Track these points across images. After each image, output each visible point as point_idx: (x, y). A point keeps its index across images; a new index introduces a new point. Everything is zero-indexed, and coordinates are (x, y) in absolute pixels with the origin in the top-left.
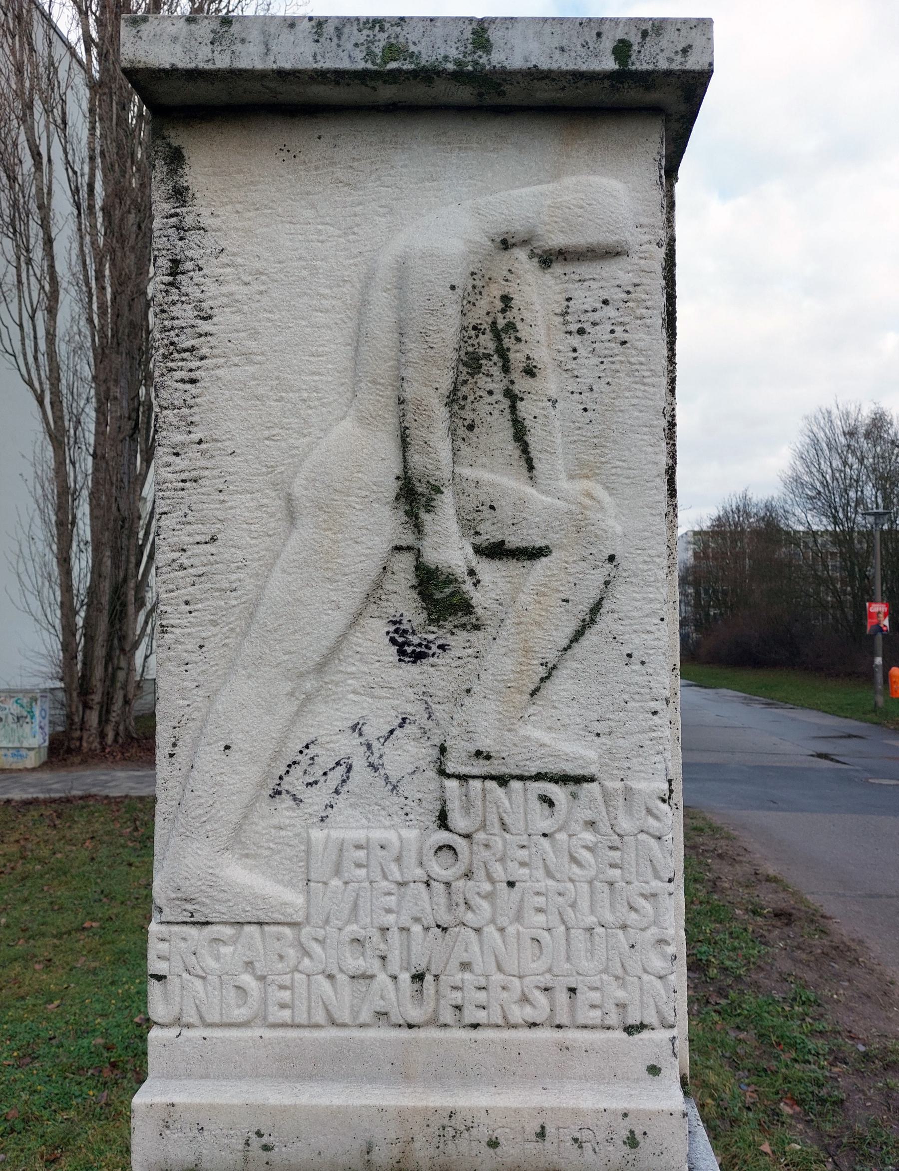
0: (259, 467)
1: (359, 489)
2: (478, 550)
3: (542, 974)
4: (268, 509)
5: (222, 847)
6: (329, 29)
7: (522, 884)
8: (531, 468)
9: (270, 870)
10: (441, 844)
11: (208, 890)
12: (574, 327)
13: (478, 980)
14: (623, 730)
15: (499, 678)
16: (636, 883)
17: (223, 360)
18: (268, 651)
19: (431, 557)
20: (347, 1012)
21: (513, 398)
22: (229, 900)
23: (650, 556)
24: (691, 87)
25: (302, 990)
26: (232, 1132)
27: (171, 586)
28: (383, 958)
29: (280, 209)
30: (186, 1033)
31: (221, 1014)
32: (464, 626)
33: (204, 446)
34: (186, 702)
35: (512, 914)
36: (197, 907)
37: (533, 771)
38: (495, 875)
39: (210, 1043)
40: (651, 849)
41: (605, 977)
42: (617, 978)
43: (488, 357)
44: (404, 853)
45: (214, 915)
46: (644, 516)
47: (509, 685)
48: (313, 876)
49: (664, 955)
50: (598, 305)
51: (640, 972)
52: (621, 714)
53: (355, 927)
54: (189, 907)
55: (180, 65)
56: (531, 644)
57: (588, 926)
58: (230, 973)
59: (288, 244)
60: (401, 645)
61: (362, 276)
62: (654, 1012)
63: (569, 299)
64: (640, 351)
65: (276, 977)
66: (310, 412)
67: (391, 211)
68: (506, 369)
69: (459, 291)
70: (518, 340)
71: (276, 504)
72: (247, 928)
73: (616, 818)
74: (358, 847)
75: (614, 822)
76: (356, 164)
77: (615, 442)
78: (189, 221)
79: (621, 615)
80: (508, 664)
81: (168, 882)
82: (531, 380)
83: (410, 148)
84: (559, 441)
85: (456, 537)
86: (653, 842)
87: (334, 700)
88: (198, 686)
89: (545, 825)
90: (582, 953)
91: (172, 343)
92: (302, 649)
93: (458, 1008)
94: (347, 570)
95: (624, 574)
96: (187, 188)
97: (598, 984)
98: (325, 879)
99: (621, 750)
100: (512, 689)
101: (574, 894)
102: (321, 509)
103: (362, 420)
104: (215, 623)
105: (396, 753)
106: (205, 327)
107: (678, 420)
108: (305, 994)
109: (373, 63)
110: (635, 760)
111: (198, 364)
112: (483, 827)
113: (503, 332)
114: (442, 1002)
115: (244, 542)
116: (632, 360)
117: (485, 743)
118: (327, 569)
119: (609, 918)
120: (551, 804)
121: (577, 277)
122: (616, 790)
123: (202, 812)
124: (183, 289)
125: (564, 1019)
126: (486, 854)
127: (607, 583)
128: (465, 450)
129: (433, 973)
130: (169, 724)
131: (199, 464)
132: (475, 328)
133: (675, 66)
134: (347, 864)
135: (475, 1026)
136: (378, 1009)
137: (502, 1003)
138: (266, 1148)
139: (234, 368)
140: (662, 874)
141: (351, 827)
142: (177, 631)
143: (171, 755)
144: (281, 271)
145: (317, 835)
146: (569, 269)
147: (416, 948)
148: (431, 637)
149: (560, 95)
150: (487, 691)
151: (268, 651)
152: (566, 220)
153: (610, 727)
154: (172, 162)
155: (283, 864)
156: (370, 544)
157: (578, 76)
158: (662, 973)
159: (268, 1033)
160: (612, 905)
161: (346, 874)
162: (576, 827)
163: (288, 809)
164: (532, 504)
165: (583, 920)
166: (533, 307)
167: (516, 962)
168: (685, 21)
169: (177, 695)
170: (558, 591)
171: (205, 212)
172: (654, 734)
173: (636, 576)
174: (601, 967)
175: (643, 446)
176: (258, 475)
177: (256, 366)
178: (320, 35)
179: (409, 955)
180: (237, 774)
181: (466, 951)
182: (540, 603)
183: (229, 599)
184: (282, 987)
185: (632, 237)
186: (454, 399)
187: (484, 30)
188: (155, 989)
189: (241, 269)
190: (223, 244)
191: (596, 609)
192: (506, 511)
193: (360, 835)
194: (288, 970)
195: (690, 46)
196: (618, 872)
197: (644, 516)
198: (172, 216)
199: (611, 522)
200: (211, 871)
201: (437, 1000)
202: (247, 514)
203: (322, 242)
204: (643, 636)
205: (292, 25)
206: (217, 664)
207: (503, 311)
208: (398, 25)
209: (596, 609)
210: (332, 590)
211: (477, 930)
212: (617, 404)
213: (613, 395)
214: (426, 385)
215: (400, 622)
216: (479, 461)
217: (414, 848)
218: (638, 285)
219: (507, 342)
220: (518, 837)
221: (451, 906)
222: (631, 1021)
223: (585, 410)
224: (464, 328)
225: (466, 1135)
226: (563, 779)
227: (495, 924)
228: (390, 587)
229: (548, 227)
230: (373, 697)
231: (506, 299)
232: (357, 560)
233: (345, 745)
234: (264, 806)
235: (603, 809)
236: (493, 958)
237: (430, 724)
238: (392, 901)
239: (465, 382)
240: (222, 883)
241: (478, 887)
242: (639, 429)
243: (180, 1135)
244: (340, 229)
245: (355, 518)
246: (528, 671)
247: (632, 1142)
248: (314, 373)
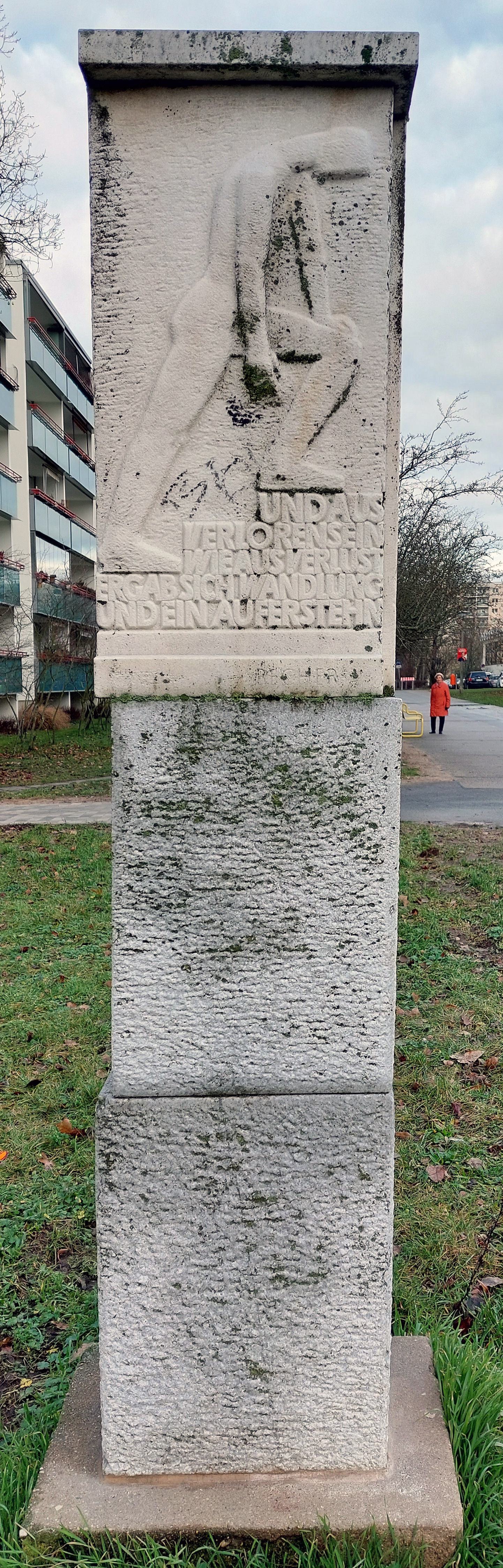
2: (280, 358)
6: (199, 38)
8: (311, 307)
12: (337, 221)
17: (132, 242)
19: (253, 360)
20: (206, 619)
21: (301, 264)
24: (408, 73)
27: (103, 381)
28: (225, 591)
32: (271, 403)
33: (120, 295)
35: (295, 566)
42: (351, 601)
43: (287, 239)
48: (186, 547)
49: (376, 588)
50: (352, 207)
51: (363, 597)
53: (209, 575)
54: (119, 563)
55: (113, 61)
60: (235, 415)
63: (334, 203)
64: (375, 236)
68: (297, 247)
69: (271, 199)
70: (305, 228)
71: (163, 330)
72: (150, 575)
74: (211, 531)
76: (211, 119)
77: (359, 291)
78: (112, 155)
79: (360, 396)
80: (296, 425)
82: (312, 253)
84: (327, 290)
85: (267, 348)
89: (315, 518)
91: (102, 232)
96: (110, 134)
104: (128, 403)
106: (121, 221)
107: (404, 282)
109: (225, 60)
111: (117, 244)
113: (296, 223)
117: (281, 471)
118: (193, 368)
119: (347, 568)
120: (318, 506)
121: (339, 190)
124: (109, 198)
125: (321, 622)
126: (281, 534)
127: (353, 377)
128: (273, 296)
131: (118, 306)
132: (279, 221)
133: (397, 62)
134: (206, 540)
135: (274, 627)
138: (166, 681)
141: (206, 519)
143: (105, 480)
145: (188, 524)
146: (335, 185)
147: (242, 586)
148: (252, 410)
149: (332, 76)
154: (101, 117)
156: (217, 353)
157: (341, 67)
159: (162, 632)
162: (332, 518)
163: (171, 511)
164: (311, 329)
168: (403, 34)
171: (121, 149)
173: (369, 373)
178: (194, 42)
179: (239, 590)
184: (170, 608)
185: (371, 165)
186: (267, 265)
187: (288, 39)
188: (100, 608)
190: (132, 169)
191: (346, 392)
192: (296, 333)
193: (212, 524)
195: (405, 50)
198: (101, 151)
199: (355, 339)
201: (254, 614)
205: (177, 36)
207: (296, 210)
208: (239, 36)
209: (346, 392)
215: (234, 402)
216: (281, 303)
217: (242, 530)
219: (298, 230)
222: (358, 623)
223: (343, 272)
224: (273, 221)
225: (270, 673)
226: (326, 491)
231: (298, 203)
232: (210, 362)
234: (158, 509)
235: (346, 507)
237: (251, 462)
238: (230, 561)
239: (273, 254)
247: (355, 675)
248: (185, 250)
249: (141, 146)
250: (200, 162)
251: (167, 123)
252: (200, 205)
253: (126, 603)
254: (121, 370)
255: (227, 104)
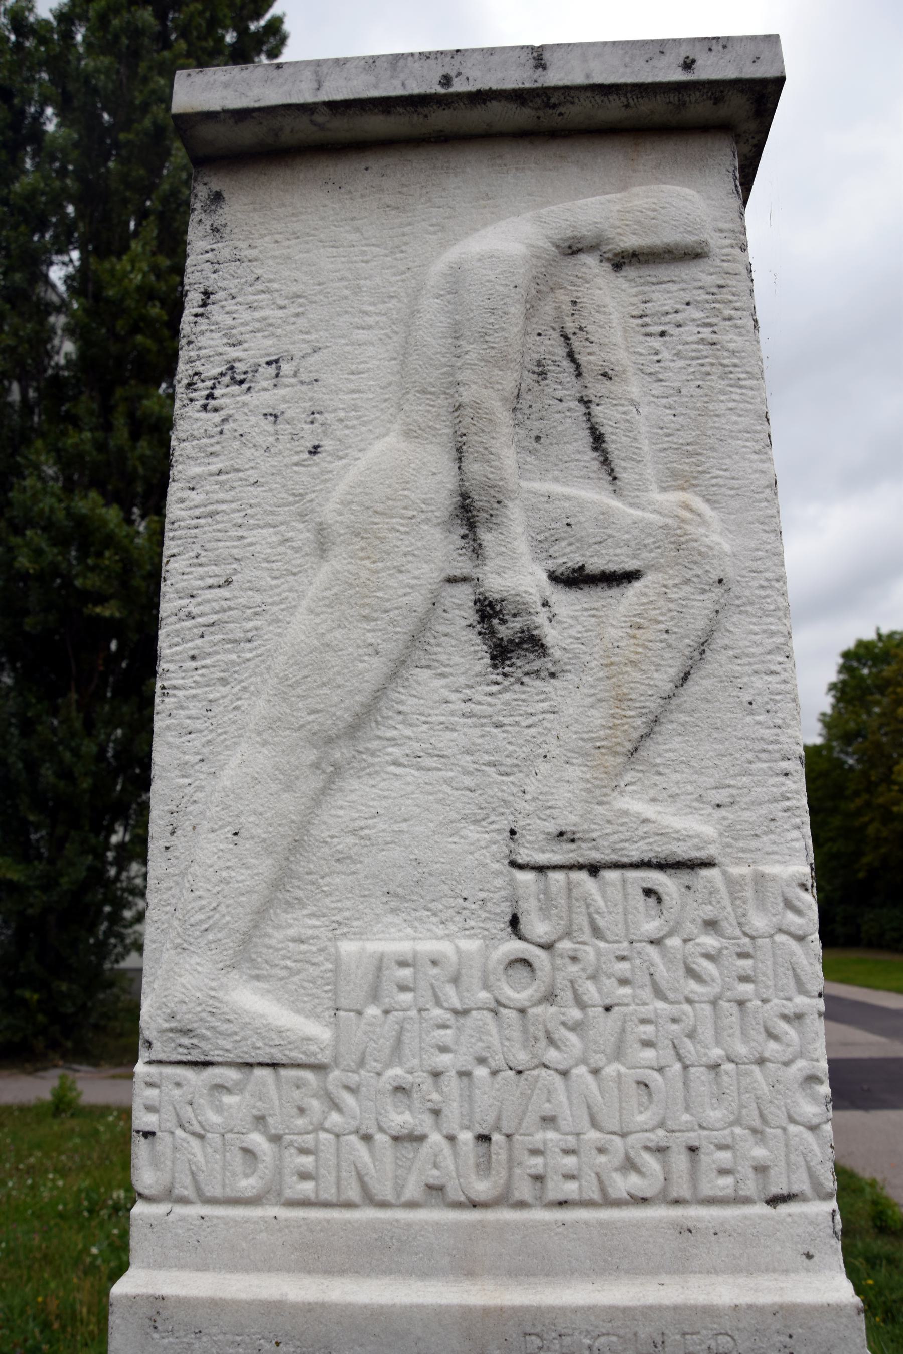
0: (285, 496)
1: (405, 508)
2: (554, 577)
3: (652, 1130)
4: (294, 544)
5: (228, 963)
7: (622, 1009)
9: (287, 996)
10: (512, 958)
11: (209, 1018)
13: (566, 1141)
14: (747, 799)
15: (586, 736)
16: (775, 1001)
18: (288, 711)
20: (389, 1184)
22: (236, 1033)
23: (767, 580)
25: (328, 1154)
26: (239, 1339)
27: (177, 640)
29: (322, 236)
30: (180, 1210)
31: (224, 1186)
33: (223, 478)
34: (187, 781)
36: (195, 1041)
37: (635, 856)
38: (585, 998)
39: (209, 1224)
40: (792, 954)
41: (738, 1130)
42: (754, 1131)
44: (463, 971)
45: (217, 1052)
46: (755, 532)
47: (598, 744)
51: (784, 1122)
52: (745, 779)
54: (186, 1041)
56: (625, 690)
57: (712, 1062)
58: (236, 1130)
59: (330, 266)
61: (410, 291)
62: (805, 1176)
65: (295, 1137)
66: (347, 432)
67: (443, 228)
72: (259, 1072)
73: (744, 915)
74: (403, 964)
75: (743, 920)
77: (713, 449)
81: (159, 1008)
83: (463, 172)
86: (794, 945)
87: (369, 774)
88: (202, 760)
89: (651, 926)
90: (707, 1099)
92: (331, 706)
93: (538, 1179)
94: (388, 605)
95: (737, 602)
97: (729, 1141)
98: (358, 1007)
99: (746, 826)
100: (603, 750)
101: (692, 1019)
102: (357, 535)
103: (408, 434)
104: (224, 682)
105: (450, 840)
108: (333, 1161)
110: (765, 839)
112: (568, 934)
114: (518, 1171)
115: (264, 583)
116: (725, 361)
117: (569, 820)
118: (364, 605)
119: (742, 1050)
122: (743, 876)
123: (203, 917)
124: (213, 319)
125: (681, 1189)
129: (504, 1131)
130: (166, 808)
131: (215, 497)
134: (388, 987)
135: (562, 1203)
136: (431, 1181)
137: (599, 1170)
139: (262, 393)
140: (809, 987)
142: (180, 693)
144: (320, 292)
150: (569, 754)
151: (288, 711)
152: (639, 222)
153: (732, 796)
155: (304, 988)
158: (815, 1121)
160: (744, 1033)
161: (387, 1000)
162: (690, 928)
165: (706, 1054)
166: (606, 310)
167: (617, 1114)
169: (177, 772)
170: (659, 622)
172: (788, 804)
174: (732, 1117)
175: (746, 453)
176: (284, 505)
177: (288, 389)
180: (248, 868)
181: (549, 1101)
182: (634, 637)
183: (243, 651)
184: (304, 1151)
188: (141, 1150)
189: (276, 295)
190: (259, 272)
191: (702, 648)
193: (404, 947)
194: (310, 1128)
196: (749, 988)
197: (755, 532)
199: (716, 538)
200: (213, 993)
201: (510, 1169)
202: (269, 551)
203: (367, 262)
204: (766, 677)
206: (225, 733)
209: (702, 648)
210: (369, 631)
211: (565, 1073)
212: (711, 407)
213: (706, 399)
214: (486, 387)
218: (722, 287)
220: (616, 945)
221: (529, 1040)
222: (775, 1190)
227: (588, 1064)
228: (440, 628)
229: (619, 230)
230: (420, 769)
232: (401, 592)
233: (383, 831)
236: (585, 1111)
238: (446, 1036)
240: (226, 1010)
241: (564, 1014)
242: (740, 435)
243: (171, 1340)
244: (385, 249)
245: (399, 543)
246: (623, 725)
248: (353, 391)
249: (277, 237)
250: (383, 251)
251: (327, 202)
252: (384, 319)
253: (201, 1137)
254: (215, 617)
255: (434, 168)
